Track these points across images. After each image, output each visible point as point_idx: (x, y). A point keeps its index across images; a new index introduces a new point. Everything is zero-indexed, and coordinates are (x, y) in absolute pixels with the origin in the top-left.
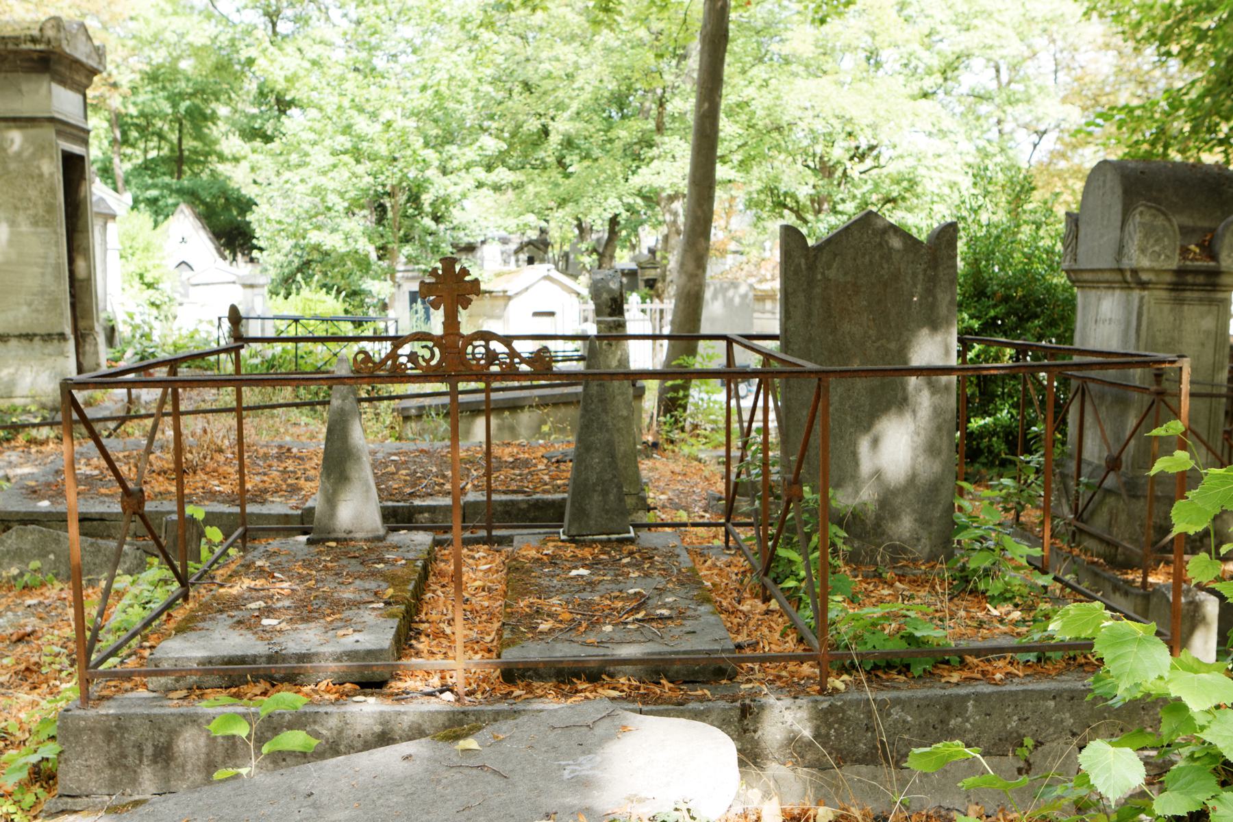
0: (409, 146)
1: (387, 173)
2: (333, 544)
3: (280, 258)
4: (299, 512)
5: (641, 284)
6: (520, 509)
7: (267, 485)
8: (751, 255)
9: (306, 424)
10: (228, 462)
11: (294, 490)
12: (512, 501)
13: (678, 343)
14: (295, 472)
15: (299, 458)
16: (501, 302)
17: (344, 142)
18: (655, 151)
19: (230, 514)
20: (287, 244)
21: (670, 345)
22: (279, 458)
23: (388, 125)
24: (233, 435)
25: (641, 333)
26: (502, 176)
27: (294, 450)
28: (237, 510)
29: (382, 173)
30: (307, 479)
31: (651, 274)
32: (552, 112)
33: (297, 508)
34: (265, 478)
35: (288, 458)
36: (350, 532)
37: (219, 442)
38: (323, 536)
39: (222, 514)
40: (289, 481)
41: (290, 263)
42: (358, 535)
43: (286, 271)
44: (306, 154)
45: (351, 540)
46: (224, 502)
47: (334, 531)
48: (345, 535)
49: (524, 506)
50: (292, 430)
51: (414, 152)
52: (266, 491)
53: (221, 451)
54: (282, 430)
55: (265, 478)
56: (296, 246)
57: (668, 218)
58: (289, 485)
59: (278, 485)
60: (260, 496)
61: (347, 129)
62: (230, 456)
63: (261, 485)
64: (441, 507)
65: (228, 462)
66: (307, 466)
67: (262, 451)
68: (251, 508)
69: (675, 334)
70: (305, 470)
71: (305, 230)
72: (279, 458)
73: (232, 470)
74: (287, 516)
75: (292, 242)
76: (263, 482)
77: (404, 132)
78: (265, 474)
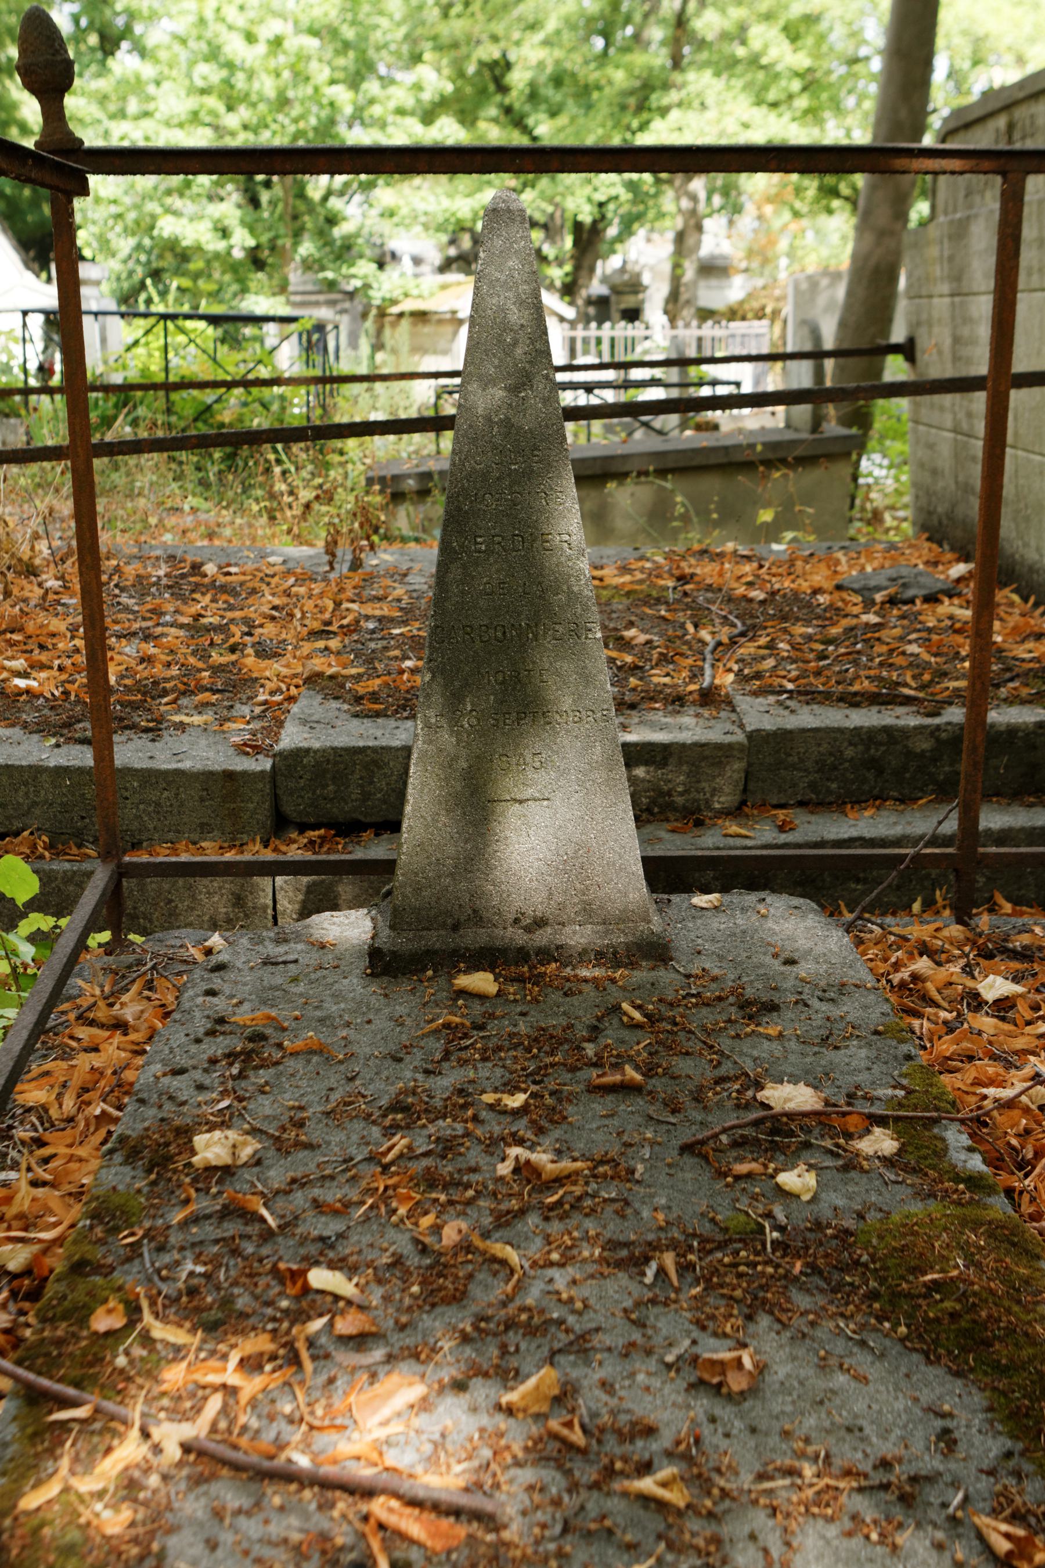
0: (308, 79)
1: (274, 126)
2: (482, 981)
3: (115, 265)
4: (267, 764)
5: (616, 315)
6: (909, 754)
7: (158, 670)
8: (807, 260)
9: (194, 510)
10: (49, 603)
11: (236, 685)
12: (887, 730)
13: (851, 361)
14: (222, 628)
15: (224, 589)
16: (449, 329)
17: (208, 73)
18: (673, 96)
19: (61, 771)
20: (125, 245)
21: (837, 366)
22: (174, 587)
23: (277, 43)
24: (64, 534)
25: (744, 352)
26: (447, 131)
27: (210, 569)
28: (83, 757)
29: (266, 126)
30: (263, 652)
31: (628, 302)
32: (516, 35)
33: (258, 750)
34: (151, 649)
35: (196, 588)
36: (540, 923)
37: (24, 551)
38: (435, 939)
39: (36, 771)
40: (217, 657)
41: (131, 273)
42: (578, 936)
43: (126, 285)
44: (150, 99)
45: (546, 954)
46: (42, 728)
47: (477, 918)
48: (519, 937)
49: (924, 745)
50: (171, 521)
51: (316, 89)
52: (155, 690)
53: (30, 571)
54: (153, 521)
55: (151, 649)
56: (139, 247)
57: (685, 204)
58: (217, 670)
59: (188, 671)
60: (142, 707)
61: (213, 54)
62: (52, 583)
63: (143, 672)
64: (683, 746)
65: (49, 603)
66: (250, 612)
67: (131, 570)
68: (130, 752)
69: (846, 346)
70: (248, 622)
71: (154, 217)
72: (174, 587)
73: (63, 625)
74: (229, 776)
75: (132, 242)
76: (146, 660)
77: (303, 57)
78: (147, 637)
